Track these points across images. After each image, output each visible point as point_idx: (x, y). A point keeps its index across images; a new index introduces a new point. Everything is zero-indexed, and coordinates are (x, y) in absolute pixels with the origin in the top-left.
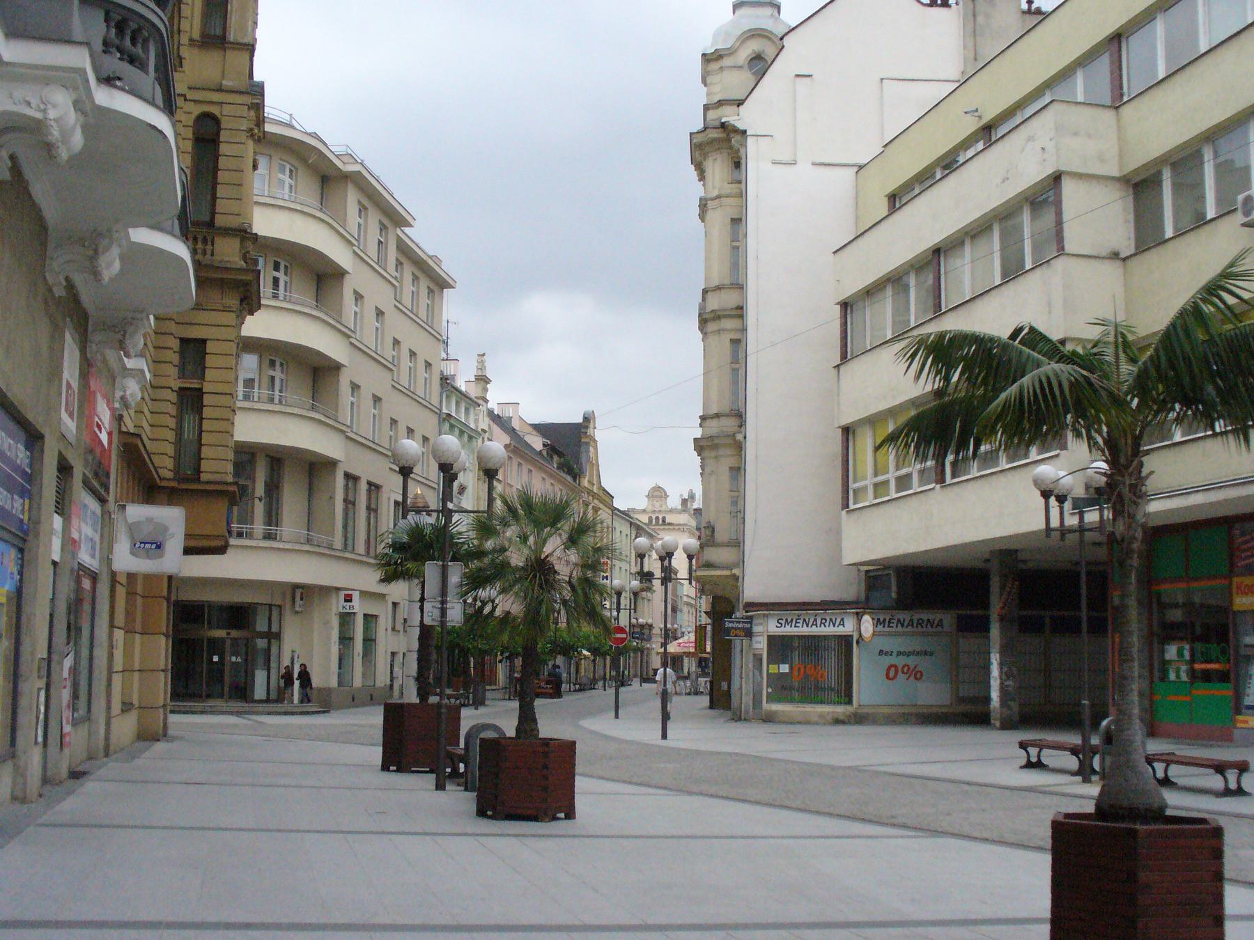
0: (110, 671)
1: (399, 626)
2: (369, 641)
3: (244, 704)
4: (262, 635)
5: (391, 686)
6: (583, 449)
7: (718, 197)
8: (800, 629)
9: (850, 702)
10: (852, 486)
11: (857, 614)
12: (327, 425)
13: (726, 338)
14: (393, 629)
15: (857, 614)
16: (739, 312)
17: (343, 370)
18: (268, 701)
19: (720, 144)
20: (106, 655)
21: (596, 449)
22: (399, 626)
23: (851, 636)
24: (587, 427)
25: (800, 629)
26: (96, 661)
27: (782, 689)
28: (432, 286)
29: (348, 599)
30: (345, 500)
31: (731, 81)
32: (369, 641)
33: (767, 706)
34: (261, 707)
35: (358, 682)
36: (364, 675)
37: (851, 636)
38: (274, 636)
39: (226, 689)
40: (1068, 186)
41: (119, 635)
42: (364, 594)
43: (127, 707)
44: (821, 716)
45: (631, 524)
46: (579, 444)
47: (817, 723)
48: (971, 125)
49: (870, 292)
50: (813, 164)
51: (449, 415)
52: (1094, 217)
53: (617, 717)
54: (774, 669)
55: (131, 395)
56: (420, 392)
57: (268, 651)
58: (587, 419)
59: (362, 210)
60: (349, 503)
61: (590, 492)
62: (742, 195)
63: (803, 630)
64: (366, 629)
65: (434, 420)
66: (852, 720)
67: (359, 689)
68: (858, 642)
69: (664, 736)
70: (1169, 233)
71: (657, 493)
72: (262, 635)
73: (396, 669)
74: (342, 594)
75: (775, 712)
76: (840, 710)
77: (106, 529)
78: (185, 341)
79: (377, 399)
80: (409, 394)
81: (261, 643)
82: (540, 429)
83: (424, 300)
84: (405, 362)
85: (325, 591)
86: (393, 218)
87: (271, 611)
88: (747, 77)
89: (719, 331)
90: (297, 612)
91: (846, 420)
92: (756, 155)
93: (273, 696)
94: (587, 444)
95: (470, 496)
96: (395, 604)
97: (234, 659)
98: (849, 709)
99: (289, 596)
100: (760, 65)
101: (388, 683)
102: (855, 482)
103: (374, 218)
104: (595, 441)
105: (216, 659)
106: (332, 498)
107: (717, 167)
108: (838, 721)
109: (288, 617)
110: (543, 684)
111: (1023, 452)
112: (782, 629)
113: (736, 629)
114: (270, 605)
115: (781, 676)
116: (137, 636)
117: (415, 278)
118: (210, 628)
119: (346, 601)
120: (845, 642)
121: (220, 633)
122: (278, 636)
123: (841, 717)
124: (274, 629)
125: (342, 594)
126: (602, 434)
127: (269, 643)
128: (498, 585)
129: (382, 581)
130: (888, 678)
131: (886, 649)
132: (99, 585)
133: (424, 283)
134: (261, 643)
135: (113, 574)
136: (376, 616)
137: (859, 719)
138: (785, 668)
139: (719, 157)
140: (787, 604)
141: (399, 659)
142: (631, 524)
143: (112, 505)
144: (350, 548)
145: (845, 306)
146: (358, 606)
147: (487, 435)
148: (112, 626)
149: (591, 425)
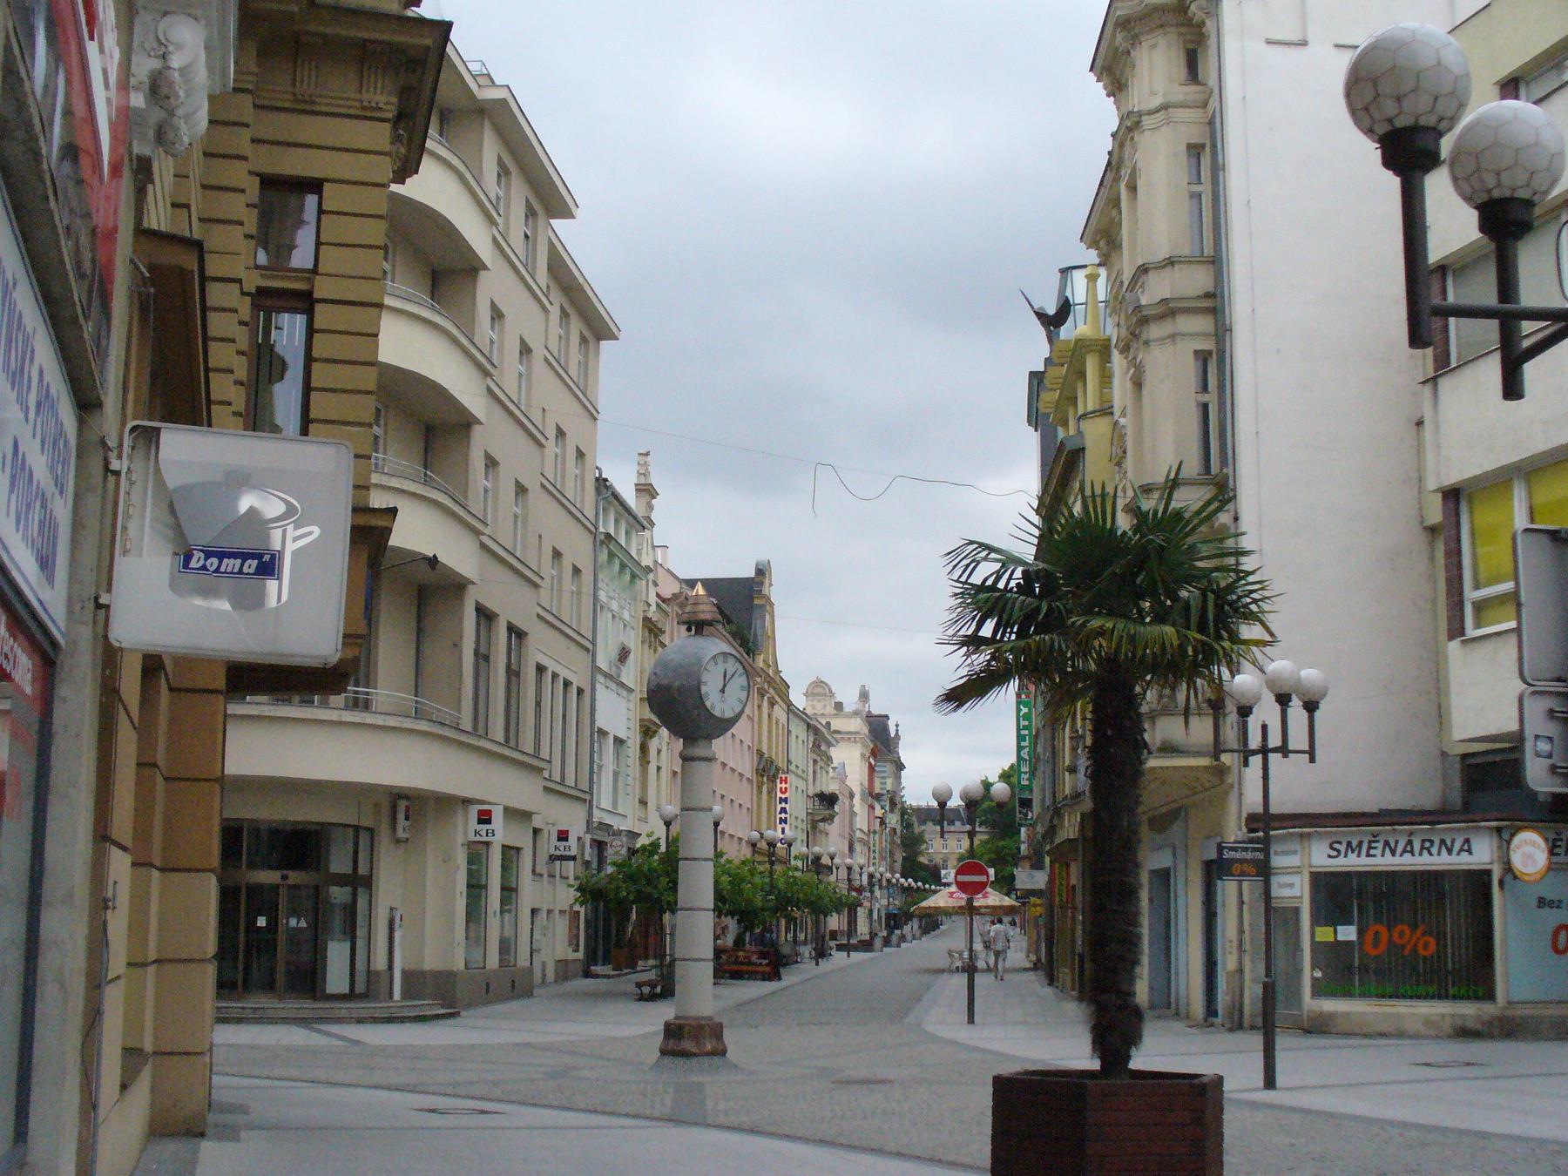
0: (96, 981)
1: (542, 868)
3: (309, 1004)
4: (341, 880)
6: (756, 613)
7: (1164, 107)
8: (1378, 860)
9: (1490, 996)
10: (1471, 595)
11: (1499, 830)
12: (454, 515)
13: (1187, 348)
15: (1499, 830)
17: (477, 429)
18: (352, 996)
20: (82, 930)
21: (772, 617)
23: (1488, 873)
24: (762, 583)
25: (1378, 860)
26: (49, 963)
27: (1342, 973)
28: (587, 333)
29: (485, 818)
30: (477, 653)
33: (1311, 1004)
34: (342, 1009)
37: (1488, 873)
38: (361, 882)
39: (281, 970)
41: (120, 864)
42: (510, 813)
43: (133, 1056)
44: (1428, 1022)
45: (809, 725)
47: (1416, 1036)
50: (1337, 46)
51: (608, 536)
53: (971, 1020)
54: (1325, 934)
55: (183, 71)
57: (350, 911)
58: (762, 572)
59: (503, 172)
60: (482, 658)
63: (1383, 861)
65: (587, 542)
66: (1496, 1031)
67: (494, 972)
68: (1501, 883)
69: (1270, 1083)
70: (1454, 364)
71: (817, 690)
72: (341, 880)
74: (473, 811)
75: (1331, 1015)
76: (1468, 1010)
77: (93, 502)
78: (270, 183)
81: (338, 894)
83: (575, 356)
86: (549, 200)
87: (357, 838)
89: (1173, 337)
90: (398, 841)
91: (1452, 478)
93: (360, 987)
94: (762, 607)
96: (536, 831)
97: (293, 922)
98: (1488, 1009)
99: (386, 810)
102: (1477, 587)
103: (519, 194)
105: (262, 922)
106: (457, 646)
108: (1464, 1033)
109: (384, 844)
112: (1341, 861)
113: (1242, 861)
114: (357, 828)
115: (1337, 945)
116: (156, 873)
118: (252, 865)
119: (480, 821)
120: (1478, 885)
121: (268, 877)
122: (368, 882)
123: (1470, 1024)
124: (363, 870)
125: (473, 811)
126: (777, 591)
127: (354, 895)
128: (1146, 726)
130: (1556, 950)
131: (1549, 896)
132: (63, 690)
133: (576, 326)
134: (338, 894)
135: (110, 656)
136: (518, 850)
137: (1508, 1029)
138: (1348, 933)
139: (1162, 42)
140: (1325, 816)
142: (809, 725)
143: (110, 420)
144: (481, 732)
146: (500, 832)
147: (651, 576)
148: (103, 836)
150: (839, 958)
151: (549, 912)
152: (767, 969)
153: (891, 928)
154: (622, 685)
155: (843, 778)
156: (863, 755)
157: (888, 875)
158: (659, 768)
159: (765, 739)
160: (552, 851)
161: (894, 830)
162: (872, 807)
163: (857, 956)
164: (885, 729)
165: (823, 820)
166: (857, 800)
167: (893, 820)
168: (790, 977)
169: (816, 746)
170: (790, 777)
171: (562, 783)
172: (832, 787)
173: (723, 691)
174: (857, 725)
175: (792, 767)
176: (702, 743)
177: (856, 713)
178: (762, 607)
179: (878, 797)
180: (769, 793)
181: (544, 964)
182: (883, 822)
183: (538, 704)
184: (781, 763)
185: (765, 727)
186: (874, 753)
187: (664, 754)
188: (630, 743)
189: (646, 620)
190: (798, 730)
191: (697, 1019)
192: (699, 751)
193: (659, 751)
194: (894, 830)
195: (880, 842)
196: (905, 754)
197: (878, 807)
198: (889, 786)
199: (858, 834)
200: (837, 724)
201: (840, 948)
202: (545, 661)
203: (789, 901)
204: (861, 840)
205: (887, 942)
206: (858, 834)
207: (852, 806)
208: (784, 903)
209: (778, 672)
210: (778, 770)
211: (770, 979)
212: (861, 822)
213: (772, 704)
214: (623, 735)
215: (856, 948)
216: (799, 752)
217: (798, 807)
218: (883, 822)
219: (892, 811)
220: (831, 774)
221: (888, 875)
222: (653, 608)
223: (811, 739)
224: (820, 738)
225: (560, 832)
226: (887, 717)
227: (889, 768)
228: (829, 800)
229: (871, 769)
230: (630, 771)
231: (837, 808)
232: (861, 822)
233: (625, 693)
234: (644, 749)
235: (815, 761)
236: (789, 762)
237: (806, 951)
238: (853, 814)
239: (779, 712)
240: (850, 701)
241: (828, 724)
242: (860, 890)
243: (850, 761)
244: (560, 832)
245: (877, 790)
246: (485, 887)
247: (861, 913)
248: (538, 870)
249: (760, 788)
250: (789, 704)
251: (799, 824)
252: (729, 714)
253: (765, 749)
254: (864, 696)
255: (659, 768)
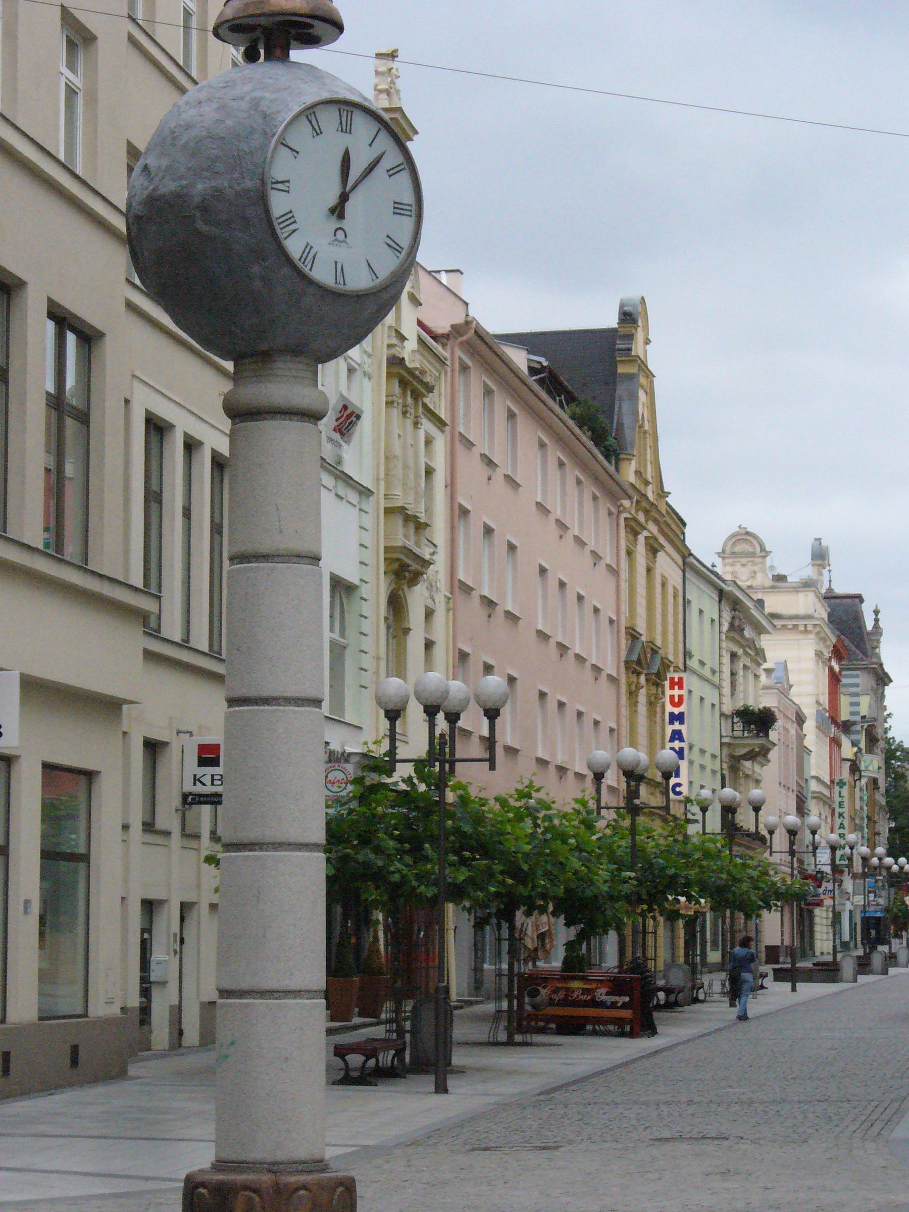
1: (167, 819)
5: (145, 1011)
6: (621, 390)
14: (149, 826)
21: (651, 394)
22: (167, 819)
24: (630, 337)
32: (64, 862)
36: (45, 977)
45: (721, 593)
46: (611, 379)
64: (54, 816)
73: (158, 955)
82: (443, 432)
95: (367, 447)
96: (153, 748)
101: (135, 1001)
104: (650, 375)
110: (601, 994)
111: (333, 825)
126: (664, 354)
129: (133, 153)
136: (89, 775)
141: (167, 922)
142: (721, 593)
149: (640, 336)
150: (776, 995)
151: (185, 908)
152: (627, 1014)
153: (871, 943)
154: (347, 480)
155: (784, 688)
156: (819, 654)
157: (864, 850)
158: (429, 645)
159: (641, 611)
160: (189, 787)
161: (875, 781)
162: (835, 742)
163: (808, 990)
164: (858, 617)
165: (751, 756)
166: (810, 726)
167: (872, 764)
168: (672, 1031)
169: (735, 628)
170: (690, 681)
171: (185, 644)
172: (762, 699)
173: (338, 211)
174: (807, 604)
175: (693, 663)
176: (284, 366)
177: (807, 585)
178: (631, 377)
179: (846, 727)
180: (651, 704)
181: (177, 1013)
182: (855, 768)
183: (187, 513)
184: (672, 653)
185: (641, 590)
186: (838, 653)
187: (440, 616)
188: (365, 591)
189: (395, 362)
190: (703, 601)
191: (273, 1167)
192: (280, 388)
193: (429, 614)
194: (875, 781)
195: (854, 799)
196: (889, 654)
197: (846, 742)
198: (864, 710)
199: (814, 786)
200: (775, 603)
201: (779, 975)
202: (165, 411)
203: (673, 884)
204: (818, 797)
205: (863, 966)
206: (814, 786)
207: (801, 738)
208: (655, 887)
209: (663, 494)
210: (666, 665)
211: (632, 1035)
212: (818, 764)
213: (653, 549)
214: (351, 575)
215: (810, 976)
216: (705, 638)
217: (705, 731)
218: (855, 768)
219: (870, 749)
220: (763, 678)
221: (864, 850)
222: (411, 344)
223: (727, 616)
224: (742, 619)
225: (203, 748)
226: (859, 598)
227: (863, 680)
228: (759, 721)
229: (834, 679)
230: (367, 643)
231: (773, 735)
232: (818, 764)
233: (353, 497)
234: (396, 604)
235: (734, 656)
236: (687, 654)
237: (715, 982)
238: (803, 751)
239: (667, 565)
240: (798, 567)
241: (760, 603)
242: (818, 878)
243: (797, 666)
244: (203, 748)
245: (844, 716)
246: (85, 858)
247: (822, 917)
248: (160, 824)
249: (632, 694)
250: (686, 555)
251: (707, 761)
252: (359, 280)
253: (641, 626)
254: (820, 556)
255: (429, 645)
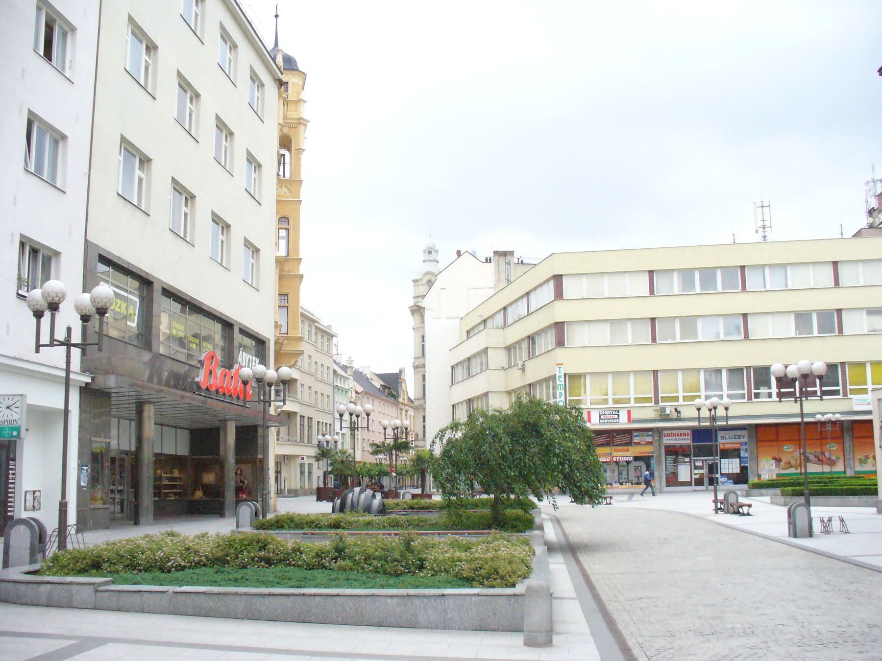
2: (310, 473)
16: (424, 366)
19: (417, 310)
29: (303, 459)
31: (422, 290)
32: (310, 473)
35: (307, 487)
40: (489, 351)
46: (398, 383)
48: (480, 320)
49: (457, 365)
52: (497, 358)
56: (326, 379)
60: (302, 425)
61: (403, 404)
62: (423, 328)
76: (72, 518)
79: (310, 356)
80: (322, 381)
82: (381, 376)
83: (326, 343)
84: (320, 369)
85: (295, 457)
88: (427, 288)
92: (427, 315)
100: (430, 283)
107: (417, 316)
117: (322, 337)
145: (453, 367)
146: (306, 461)
